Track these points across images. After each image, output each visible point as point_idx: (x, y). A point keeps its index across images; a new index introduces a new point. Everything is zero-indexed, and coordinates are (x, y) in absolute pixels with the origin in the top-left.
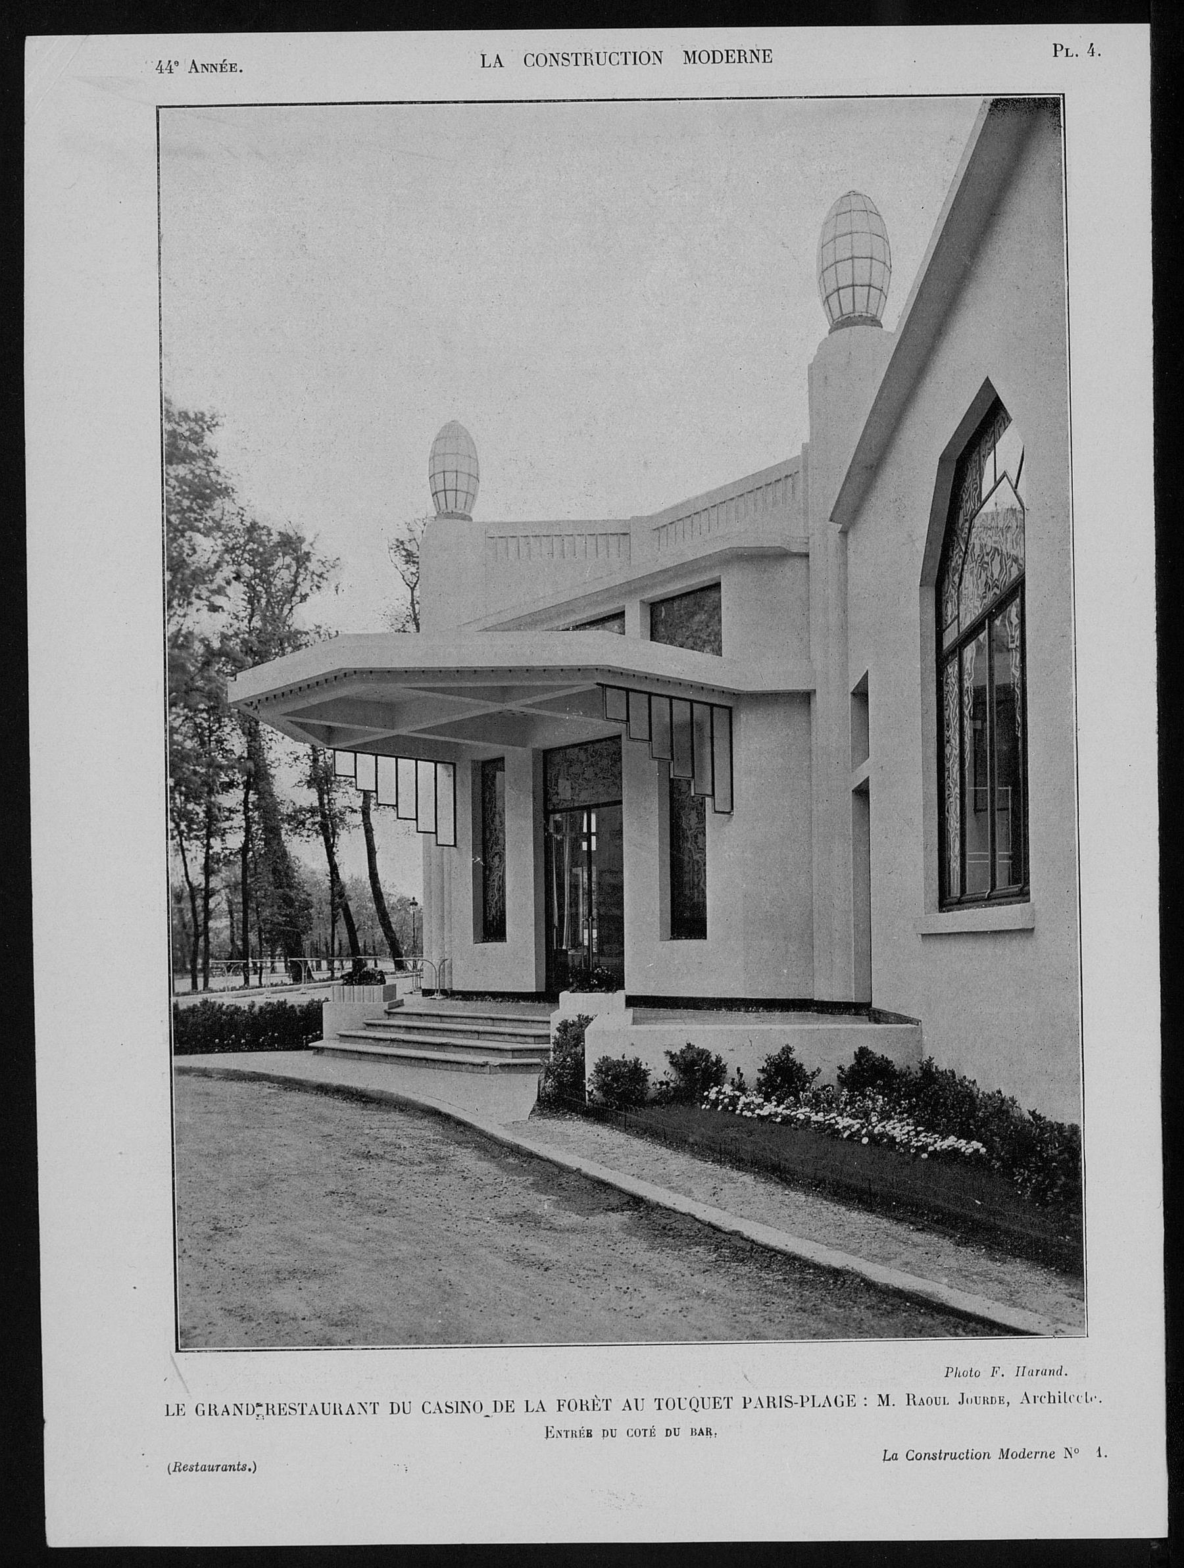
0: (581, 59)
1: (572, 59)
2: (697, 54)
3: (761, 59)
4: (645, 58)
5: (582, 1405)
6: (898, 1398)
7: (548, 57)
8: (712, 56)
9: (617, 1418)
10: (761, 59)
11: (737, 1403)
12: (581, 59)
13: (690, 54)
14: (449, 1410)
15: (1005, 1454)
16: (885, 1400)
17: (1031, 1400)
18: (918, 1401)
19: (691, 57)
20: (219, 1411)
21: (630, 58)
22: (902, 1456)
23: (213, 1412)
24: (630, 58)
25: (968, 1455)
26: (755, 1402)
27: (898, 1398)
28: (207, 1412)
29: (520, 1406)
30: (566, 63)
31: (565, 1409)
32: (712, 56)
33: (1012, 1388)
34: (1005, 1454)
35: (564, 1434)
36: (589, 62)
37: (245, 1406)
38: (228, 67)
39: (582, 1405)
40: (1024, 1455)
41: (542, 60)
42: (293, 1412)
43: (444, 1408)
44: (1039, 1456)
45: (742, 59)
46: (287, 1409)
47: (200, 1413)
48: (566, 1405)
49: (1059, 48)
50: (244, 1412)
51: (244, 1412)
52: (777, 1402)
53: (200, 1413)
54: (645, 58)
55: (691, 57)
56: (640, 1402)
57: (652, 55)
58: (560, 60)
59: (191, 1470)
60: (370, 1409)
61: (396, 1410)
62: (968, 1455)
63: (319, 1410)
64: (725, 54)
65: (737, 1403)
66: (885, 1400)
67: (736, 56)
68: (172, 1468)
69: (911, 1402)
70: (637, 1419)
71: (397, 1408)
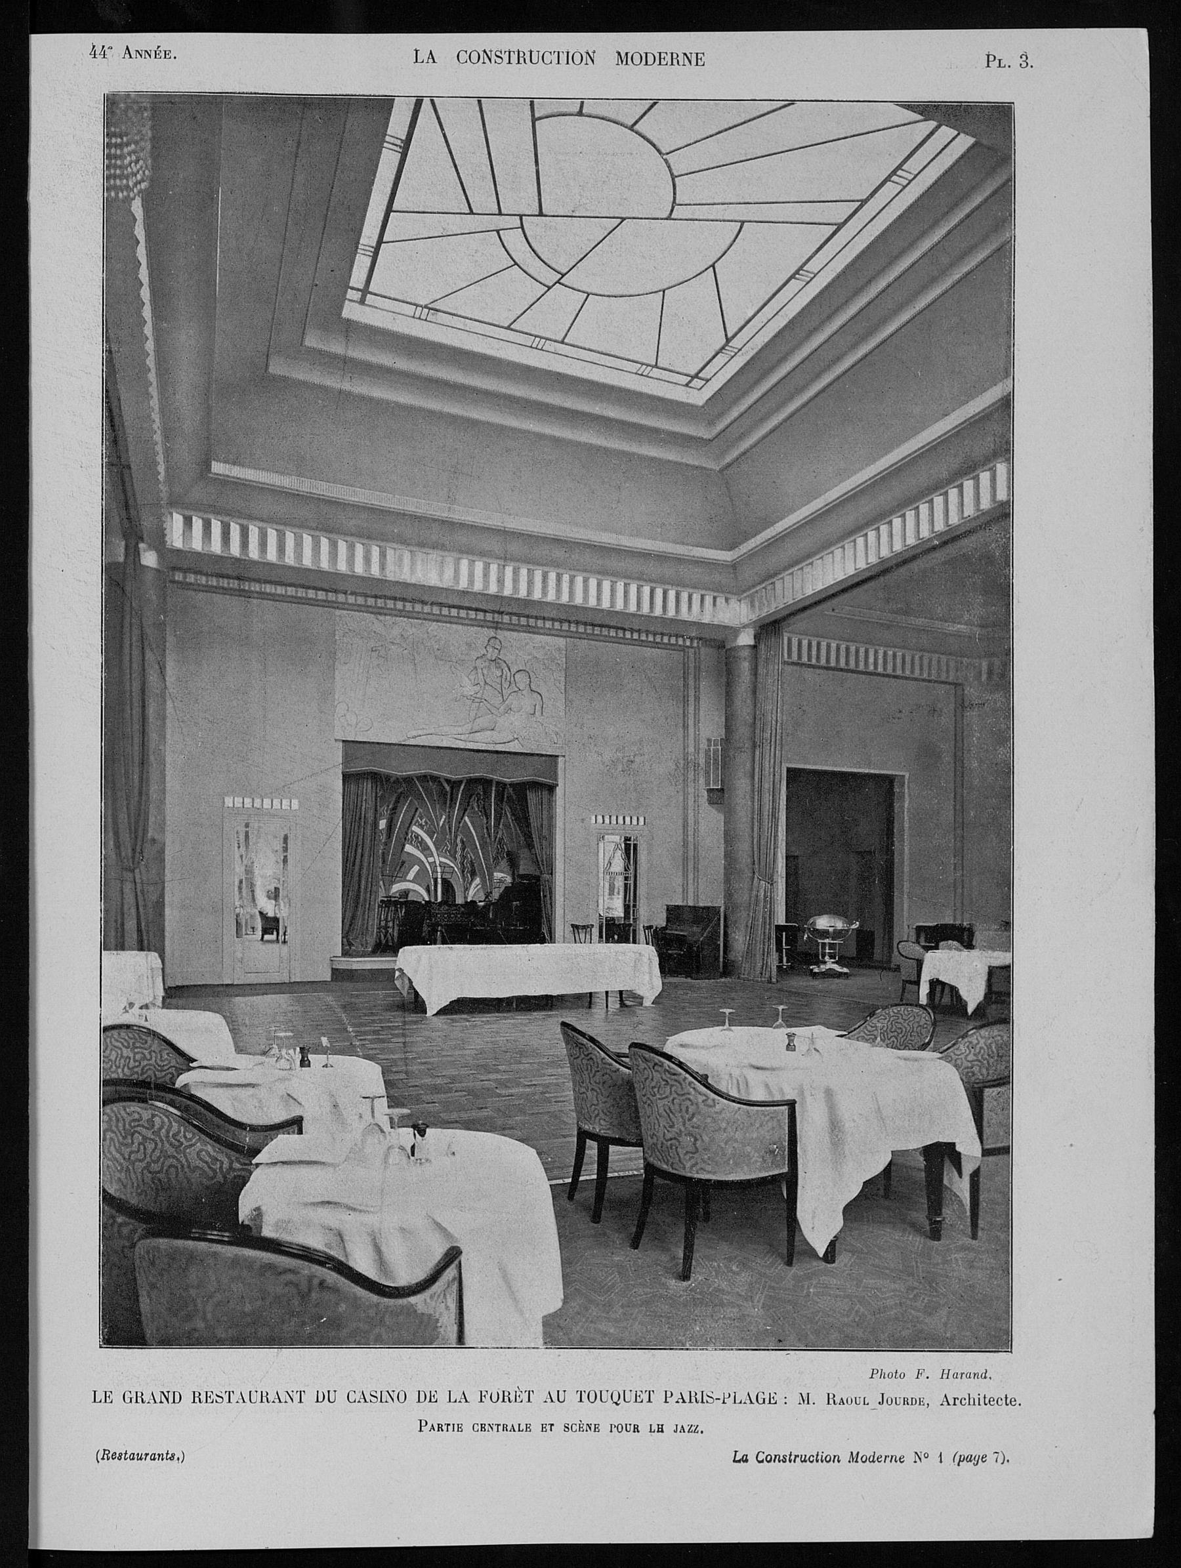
0: (514, 57)
1: (506, 57)
2: (630, 56)
3: (694, 62)
4: (577, 58)
5: (504, 1397)
6: (819, 1398)
7: (482, 54)
8: (644, 59)
9: (535, 1413)
10: (694, 62)
11: (658, 1397)
12: (514, 57)
13: (623, 55)
14: (374, 1399)
15: (854, 1458)
16: (805, 1399)
17: (951, 1402)
18: (838, 1400)
19: (623, 58)
20: (271, 1398)
21: (563, 57)
22: (752, 1458)
23: (139, 1400)
24: (563, 57)
25: (817, 1459)
26: (677, 1396)
27: (819, 1398)
28: (134, 1400)
29: (442, 1397)
30: (499, 60)
31: (487, 1400)
32: (644, 59)
33: (933, 1389)
34: (854, 1458)
35: (495, 1428)
36: (522, 60)
37: (171, 1395)
38: (163, 54)
39: (504, 1397)
40: (874, 1459)
41: (474, 57)
42: (219, 1400)
43: (368, 1398)
44: (888, 1459)
45: (675, 61)
46: (214, 1397)
47: (128, 1400)
48: (488, 1397)
49: (991, 58)
50: (171, 1400)
51: (171, 1400)
52: (203, 1398)
53: (128, 1400)
54: (577, 58)
55: (623, 58)
56: (332, 1394)
57: (482, 54)
58: (493, 58)
59: (796, 1456)
60: (296, 1397)
61: (422, 1399)
62: (817, 1459)
63: (247, 1399)
64: (657, 56)
65: (658, 1397)
66: (805, 1399)
67: (668, 58)
68: (100, 1457)
69: (831, 1401)
70: (559, 1415)
71: (325, 1397)
